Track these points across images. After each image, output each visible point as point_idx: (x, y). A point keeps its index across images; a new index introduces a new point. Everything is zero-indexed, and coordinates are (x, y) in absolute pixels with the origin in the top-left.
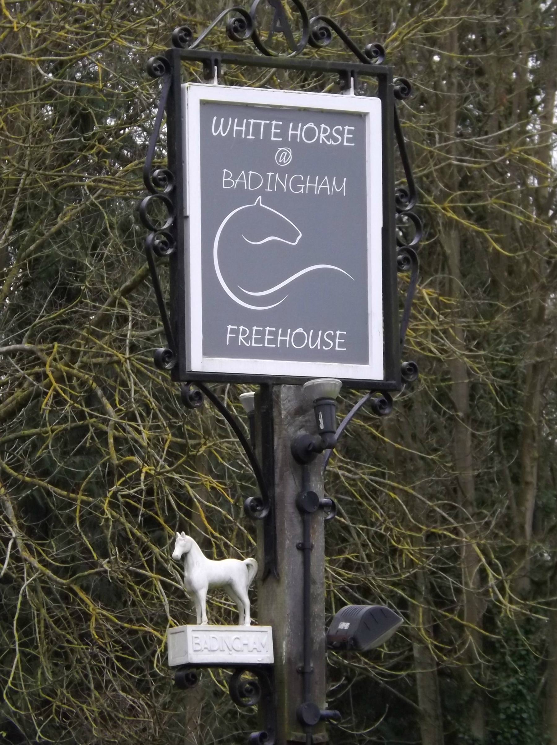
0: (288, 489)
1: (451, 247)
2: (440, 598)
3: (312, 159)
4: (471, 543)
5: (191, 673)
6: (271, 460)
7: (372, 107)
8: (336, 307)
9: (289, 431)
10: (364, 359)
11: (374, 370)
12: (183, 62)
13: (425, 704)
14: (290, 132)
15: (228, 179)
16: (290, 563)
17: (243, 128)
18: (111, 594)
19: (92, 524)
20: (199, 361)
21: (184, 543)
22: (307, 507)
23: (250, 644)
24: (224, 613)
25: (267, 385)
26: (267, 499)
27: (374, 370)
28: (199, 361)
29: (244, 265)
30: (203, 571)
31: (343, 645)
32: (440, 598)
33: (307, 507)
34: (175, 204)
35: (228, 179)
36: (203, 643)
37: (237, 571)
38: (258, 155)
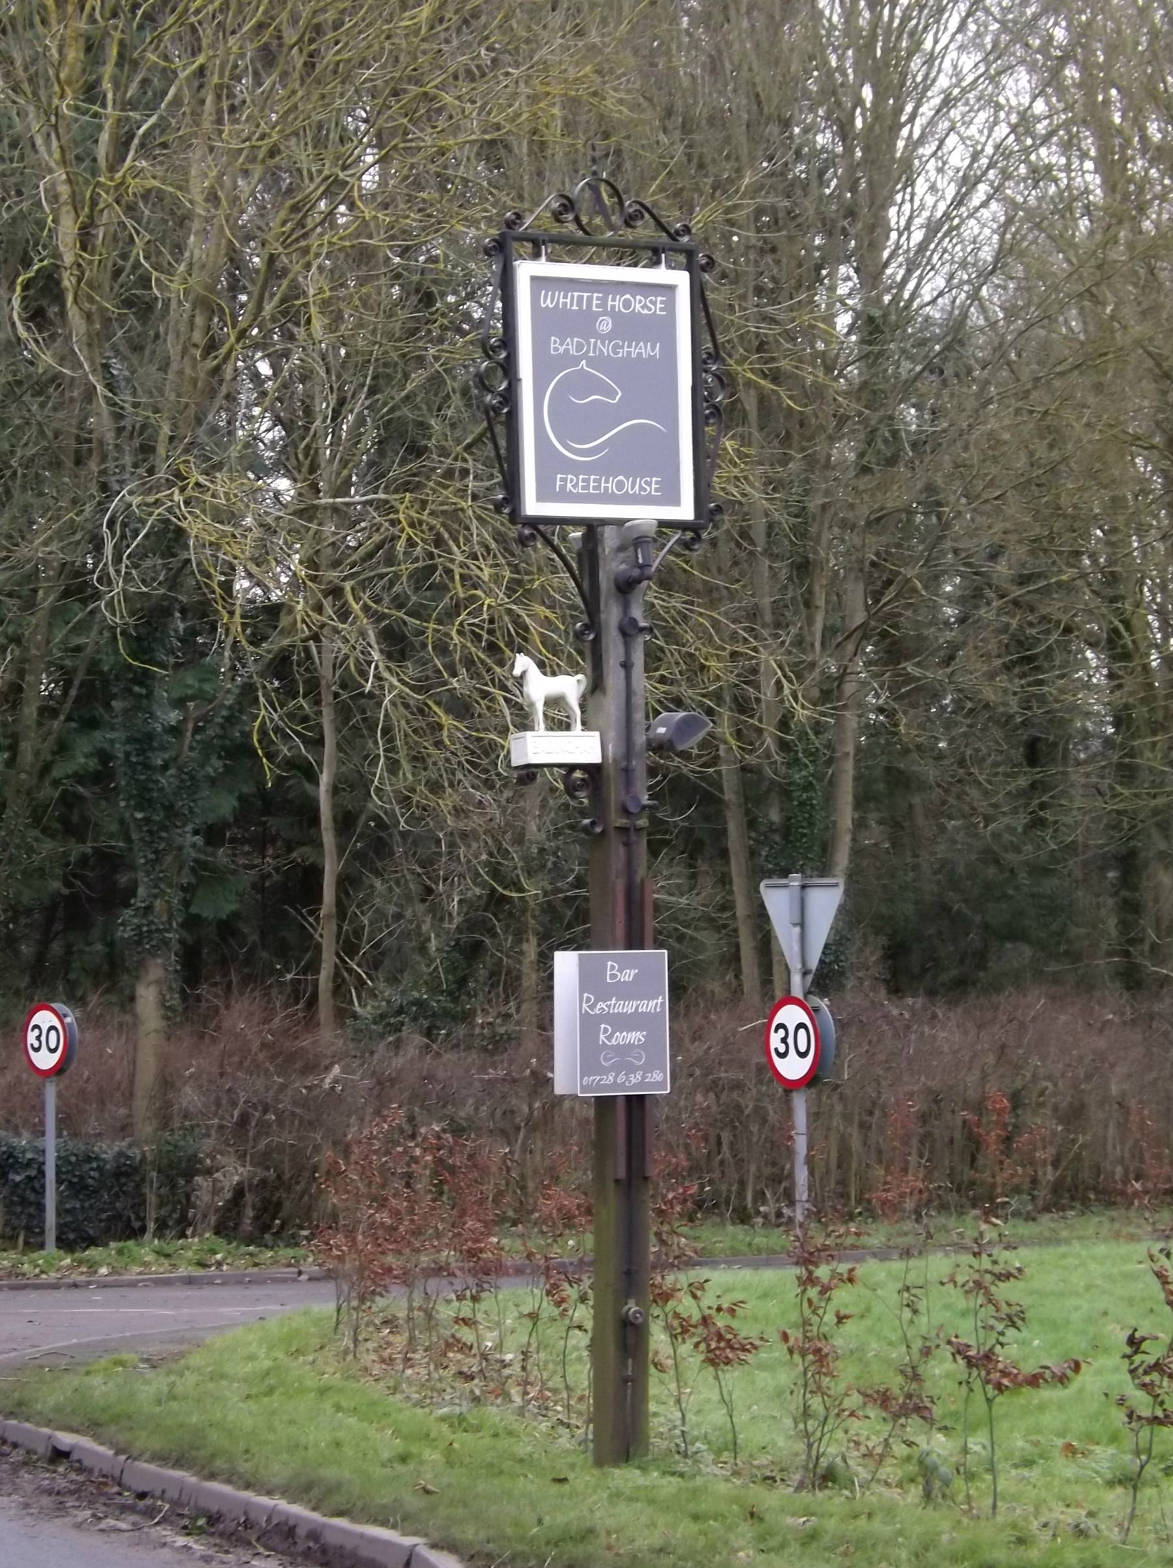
0: (611, 615)
1: (750, 403)
2: (743, 706)
3: (630, 327)
4: (769, 660)
5: (530, 773)
6: (595, 590)
7: (681, 279)
8: (645, 458)
10: (675, 501)
11: (685, 511)
13: (730, 794)
15: (556, 346)
16: (614, 678)
17: (569, 300)
18: (461, 708)
19: (442, 649)
20: (533, 506)
23: (582, 747)
25: (592, 527)
26: (594, 623)
27: (685, 511)
29: (572, 422)
30: (539, 686)
31: (660, 747)
32: (743, 706)
33: (628, 630)
35: (556, 346)
36: (538, 747)
38: (583, 324)
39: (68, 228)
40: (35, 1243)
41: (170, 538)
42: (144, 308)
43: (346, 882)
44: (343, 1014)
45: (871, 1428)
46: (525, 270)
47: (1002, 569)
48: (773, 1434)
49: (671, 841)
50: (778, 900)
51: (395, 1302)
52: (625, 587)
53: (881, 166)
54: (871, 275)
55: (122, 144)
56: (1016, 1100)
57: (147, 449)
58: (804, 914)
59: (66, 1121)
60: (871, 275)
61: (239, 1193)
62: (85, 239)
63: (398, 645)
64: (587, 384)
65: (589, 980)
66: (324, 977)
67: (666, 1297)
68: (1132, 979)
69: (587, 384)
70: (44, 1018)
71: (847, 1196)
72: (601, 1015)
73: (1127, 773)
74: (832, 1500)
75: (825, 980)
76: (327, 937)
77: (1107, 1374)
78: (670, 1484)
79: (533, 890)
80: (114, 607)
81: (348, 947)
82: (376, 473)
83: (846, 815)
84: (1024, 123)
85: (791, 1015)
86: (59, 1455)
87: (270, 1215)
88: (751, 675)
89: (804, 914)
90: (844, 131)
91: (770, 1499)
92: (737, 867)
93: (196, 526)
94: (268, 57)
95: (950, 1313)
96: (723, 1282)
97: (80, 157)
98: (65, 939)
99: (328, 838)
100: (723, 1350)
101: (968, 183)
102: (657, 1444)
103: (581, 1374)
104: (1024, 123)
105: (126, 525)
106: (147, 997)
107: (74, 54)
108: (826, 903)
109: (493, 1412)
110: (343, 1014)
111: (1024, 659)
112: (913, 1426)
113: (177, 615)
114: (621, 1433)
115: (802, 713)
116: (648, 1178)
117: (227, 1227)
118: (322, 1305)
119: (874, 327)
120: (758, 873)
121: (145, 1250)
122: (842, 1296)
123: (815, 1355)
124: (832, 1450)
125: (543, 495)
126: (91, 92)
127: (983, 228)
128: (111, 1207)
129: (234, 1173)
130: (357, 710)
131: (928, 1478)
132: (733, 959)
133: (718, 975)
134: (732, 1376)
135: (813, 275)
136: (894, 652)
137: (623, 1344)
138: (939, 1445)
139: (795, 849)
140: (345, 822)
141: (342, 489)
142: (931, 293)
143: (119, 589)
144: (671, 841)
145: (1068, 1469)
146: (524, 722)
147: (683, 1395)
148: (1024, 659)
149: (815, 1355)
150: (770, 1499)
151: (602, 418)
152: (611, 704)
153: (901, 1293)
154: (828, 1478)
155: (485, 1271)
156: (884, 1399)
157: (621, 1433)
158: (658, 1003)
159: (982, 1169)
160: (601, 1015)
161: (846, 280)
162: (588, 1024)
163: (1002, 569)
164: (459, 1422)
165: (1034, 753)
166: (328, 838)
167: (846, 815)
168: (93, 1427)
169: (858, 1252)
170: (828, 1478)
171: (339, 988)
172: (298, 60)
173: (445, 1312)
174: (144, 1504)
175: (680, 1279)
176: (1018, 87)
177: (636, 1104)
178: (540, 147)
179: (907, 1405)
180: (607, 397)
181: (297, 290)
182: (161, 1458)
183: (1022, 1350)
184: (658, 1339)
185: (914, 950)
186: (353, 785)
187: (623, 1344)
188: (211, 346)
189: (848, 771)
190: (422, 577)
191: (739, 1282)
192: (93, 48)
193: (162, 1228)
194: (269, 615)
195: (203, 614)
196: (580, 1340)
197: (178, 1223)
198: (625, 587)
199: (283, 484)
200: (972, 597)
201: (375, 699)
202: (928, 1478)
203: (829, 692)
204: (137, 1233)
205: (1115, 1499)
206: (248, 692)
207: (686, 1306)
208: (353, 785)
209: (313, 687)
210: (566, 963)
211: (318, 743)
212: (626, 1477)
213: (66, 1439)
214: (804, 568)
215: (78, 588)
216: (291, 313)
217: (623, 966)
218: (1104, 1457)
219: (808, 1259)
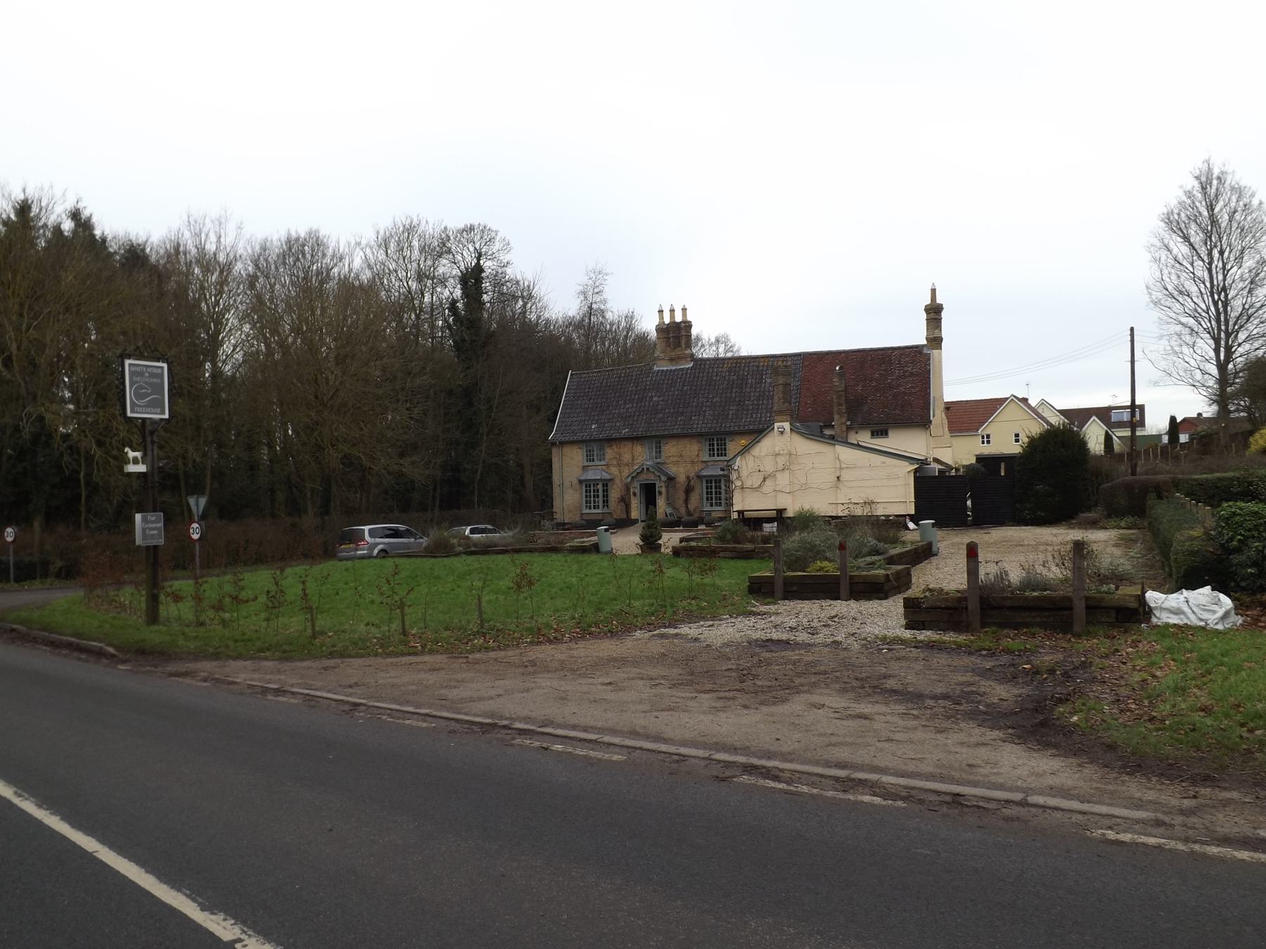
0: (149, 439)
1: (185, 392)
2: (184, 458)
3: (152, 375)
4: (191, 448)
5: (129, 474)
6: (144, 433)
7: (165, 365)
8: (158, 404)
9: (149, 428)
10: (163, 413)
11: (166, 416)
12: (982, 576)
13: (181, 476)
14: (366, 528)
15: (135, 379)
16: (149, 453)
17: (138, 369)
18: (115, 458)
19: (111, 444)
20: (129, 414)
21: (127, 449)
22: (153, 442)
23: (142, 468)
24: (136, 461)
25: (144, 419)
26: (144, 440)
27: (166, 416)
28: (129, 414)
29: (138, 395)
30: (131, 454)
31: (159, 468)
32: (184, 458)
33: (153, 442)
34: (123, 383)
35: (135, 379)
36: (131, 468)
37: (138, 454)
38: (141, 374)
39: (14, 347)
40: (8, 581)
41: (41, 419)
42: (35, 365)
43: (88, 497)
44: (87, 527)
45: (211, 613)
46: (127, 362)
47: (244, 429)
48: (189, 615)
49: (164, 490)
50: (192, 501)
51: (98, 591)
52: (152, 433)
53: (215, 343)
54: (214, 364)
55: (28, 329)
56: (247, 541)
57: (35, 398)
58: (198, 504)
59: (16, 553)
60: (214, 364)
61: (61, 569)
62: (19, 349)
63: (100, 444)
64: (142, 388)
65: (144, 520)
66: (82, 519)
67: (163, 588)
68: (273, 516)
69: (142, 388)
70: (9, 530)
71: (209, 564)
72: (146, 527)
73: (272, 472)
74: (201, 629)
75: (203, 517)
76: (83, 509)
77: (263, 599)
78: (164, 629)
79: (134, 499)
80: (26, 434)
81: (89, 511)
82: (95, 405)
83: (208, 481)
84: (248, 335)
85: (195, 525)
86: (13, 630)
87: (69, 573)
88: (186, 451)
89: (198, 504)
90: (208, 334)
91: (187, 630)
92: (183, 492)
93: (48, 416)
94: (67, 309)
95: (228, 588)
96: (177, 584)
97: (18, 329)
98: (14, 512)
99: (83, 487)
100: (177, 598)
101: (235, 347)
102: (161, 619)
103: (144, 605)
104: (248, 335)
105: (29, 415)
106: (36, 525)
107: (16, 306)
108: (203, 501)
109: (123, 615)
110: (87, 527)
111: (250, 448)
112: (221, 614)
113: (44, 435)
114: (153, 616)
115: (198, 460)
116: (155, 565)
117: (58, 575)
118: (81, 593)
119: (213, 376)
120: (188, 494)
121: (37, 583)
122: (206, 586)
123: (198, 599)
124: (202, 619)
125: (132, 411)
126: (21, 315)
127: (239, 356)
128: (28, 572)
129: (59, 564)
130: (90, 458)
131: (224, 623)
132: (182, 513)
133: (175, 518)
134: (180, 605)
135: (202, 364)
136: (220, 446)
137: (154, 600)
138: (227, 615)
139: (197, 490)
140: (88, 484)
141: (87, 407)
142: (227, 369)
143: (27, 430)
144: (164, 490)
145: (254, 618)
146: (127, 462)
147: (168, 609)
148: (250, 448)
149: (198, 599)
150: (187, 630)
151: (147, 395)
152: (149, 459)
153: (217, 585)
154: (202, 624)
155: (119, 584)
156: (213, 607)
157: (153, 616)
158: (161, 525)
159: (239, 556)
160: (146, 527)
161: (208, 365)
162: (144, 530)
163: (244, 429)
164: (114, 618)
165: (252, 468)
166: (83, 487)
167: (208, 481)
168: (22, 623)
169: (211, 576)
170: (202, 624)
171: (86, 521)
172: (74, 310)
173: (112, 593)
174: (35, 640)
175: (167, 584)
176: (247, 328)
177: (156, 547)
178: (135, 334)
179: (219, 607)
180: (146, 390)
181: (74, 363)
182: (40, 630)
183: (243, 595)
184: (162, 597)
185: (225, 510)
186: (89, 475)
187: (154, 600)
188: (52, 374)
189: (209, 473)
190: (106, 428)
191: (183, 585)
192: (21, 305)
193: (41, 577)
194: (66, 437)
195: (50, 436)
196: (143, 599)
197: (45, 575)
198: (152, 433)
199: (71, 407)
200: (238, 435)
201: (94, 456)
202: (224, 623)
203: (204, 455)
204: (35, 578)
205: (264, 624)
206: (62, 455)
207: (169, 590)
208: (89, 475)
209: (79, 454)
210: (138, 517)
211: (80, 466)
212: (155, 628)
213: (15, 626)
214: (198, 428)
215: (17, 429)
216: (72, 367)
217: (151, 517)
218: (263, 615)
219: (196, 578)
